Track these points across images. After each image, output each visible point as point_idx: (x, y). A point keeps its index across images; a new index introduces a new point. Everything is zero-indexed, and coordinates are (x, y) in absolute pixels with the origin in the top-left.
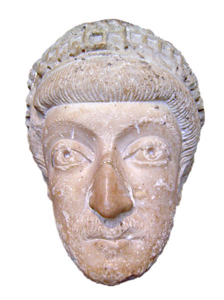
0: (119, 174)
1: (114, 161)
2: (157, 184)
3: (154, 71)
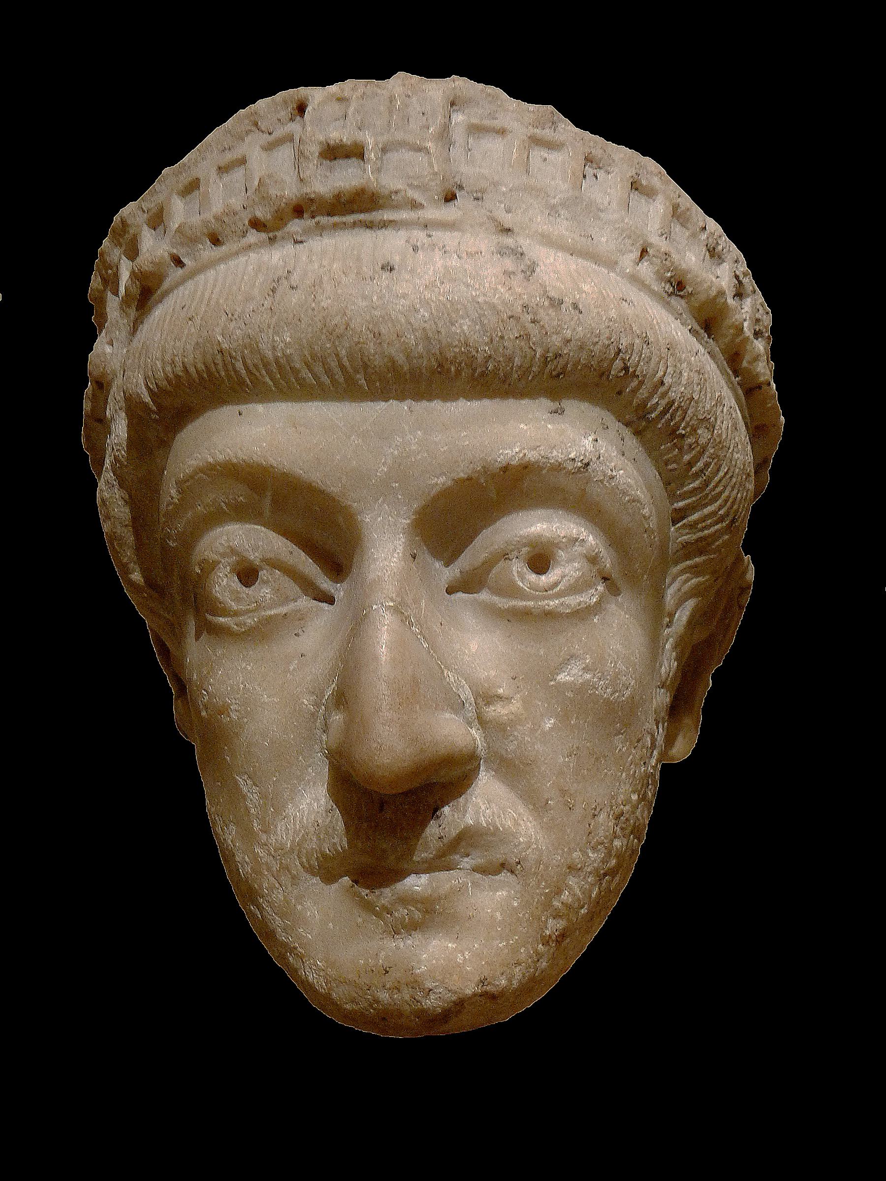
1: (409, 600)
2: (562, 677)
3: (543, 235)
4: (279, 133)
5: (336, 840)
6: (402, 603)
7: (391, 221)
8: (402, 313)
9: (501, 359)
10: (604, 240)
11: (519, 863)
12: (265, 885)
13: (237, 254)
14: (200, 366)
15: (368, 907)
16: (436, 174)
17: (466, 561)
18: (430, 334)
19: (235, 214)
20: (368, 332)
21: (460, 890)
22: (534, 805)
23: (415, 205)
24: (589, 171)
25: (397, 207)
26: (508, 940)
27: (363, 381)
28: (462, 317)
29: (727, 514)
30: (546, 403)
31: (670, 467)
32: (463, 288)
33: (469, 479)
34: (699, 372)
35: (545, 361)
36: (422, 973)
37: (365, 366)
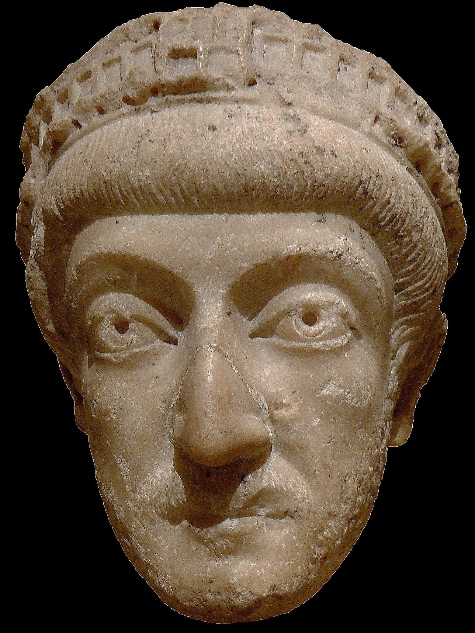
0: (236, 371)
1: (226, 342)
2: (325, 392)
3: (312, 107)
4: (142, 41)
5: (179, 497)
6: (222, 344)
7: (214, 98)
8: (221, 158)
9: (285, 187)
10: (351, 110)
11: (297, 511)
12: (133, 525)
13: (115, 119)
14: (92, 192)
15: (199, 540)
16: (243, 68)
17: (263, 316)
18: (240, 171)
19: (114, 93)
20: (200, 170)
21: (259, 529)
22: (306, 474)
23: (229, 88)
24: (342, 66)
25: (218, 89)
26: (289, 561)
27: (196, 201)
28: (260, 160)
29: (431, 287)
30: (314, 215)
31: (394, 256)
32: (261, 141)
33: (265, 264)
34: (412, 195)
35: (314, 188)
36: (234, 582)
37: (198, 192)
